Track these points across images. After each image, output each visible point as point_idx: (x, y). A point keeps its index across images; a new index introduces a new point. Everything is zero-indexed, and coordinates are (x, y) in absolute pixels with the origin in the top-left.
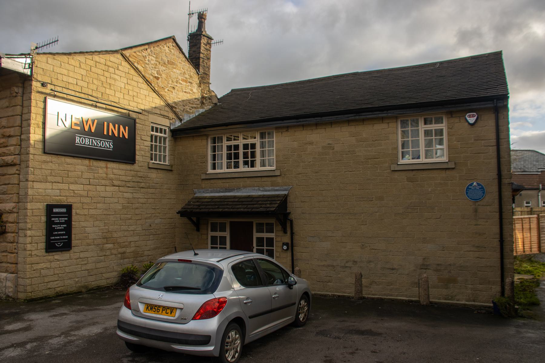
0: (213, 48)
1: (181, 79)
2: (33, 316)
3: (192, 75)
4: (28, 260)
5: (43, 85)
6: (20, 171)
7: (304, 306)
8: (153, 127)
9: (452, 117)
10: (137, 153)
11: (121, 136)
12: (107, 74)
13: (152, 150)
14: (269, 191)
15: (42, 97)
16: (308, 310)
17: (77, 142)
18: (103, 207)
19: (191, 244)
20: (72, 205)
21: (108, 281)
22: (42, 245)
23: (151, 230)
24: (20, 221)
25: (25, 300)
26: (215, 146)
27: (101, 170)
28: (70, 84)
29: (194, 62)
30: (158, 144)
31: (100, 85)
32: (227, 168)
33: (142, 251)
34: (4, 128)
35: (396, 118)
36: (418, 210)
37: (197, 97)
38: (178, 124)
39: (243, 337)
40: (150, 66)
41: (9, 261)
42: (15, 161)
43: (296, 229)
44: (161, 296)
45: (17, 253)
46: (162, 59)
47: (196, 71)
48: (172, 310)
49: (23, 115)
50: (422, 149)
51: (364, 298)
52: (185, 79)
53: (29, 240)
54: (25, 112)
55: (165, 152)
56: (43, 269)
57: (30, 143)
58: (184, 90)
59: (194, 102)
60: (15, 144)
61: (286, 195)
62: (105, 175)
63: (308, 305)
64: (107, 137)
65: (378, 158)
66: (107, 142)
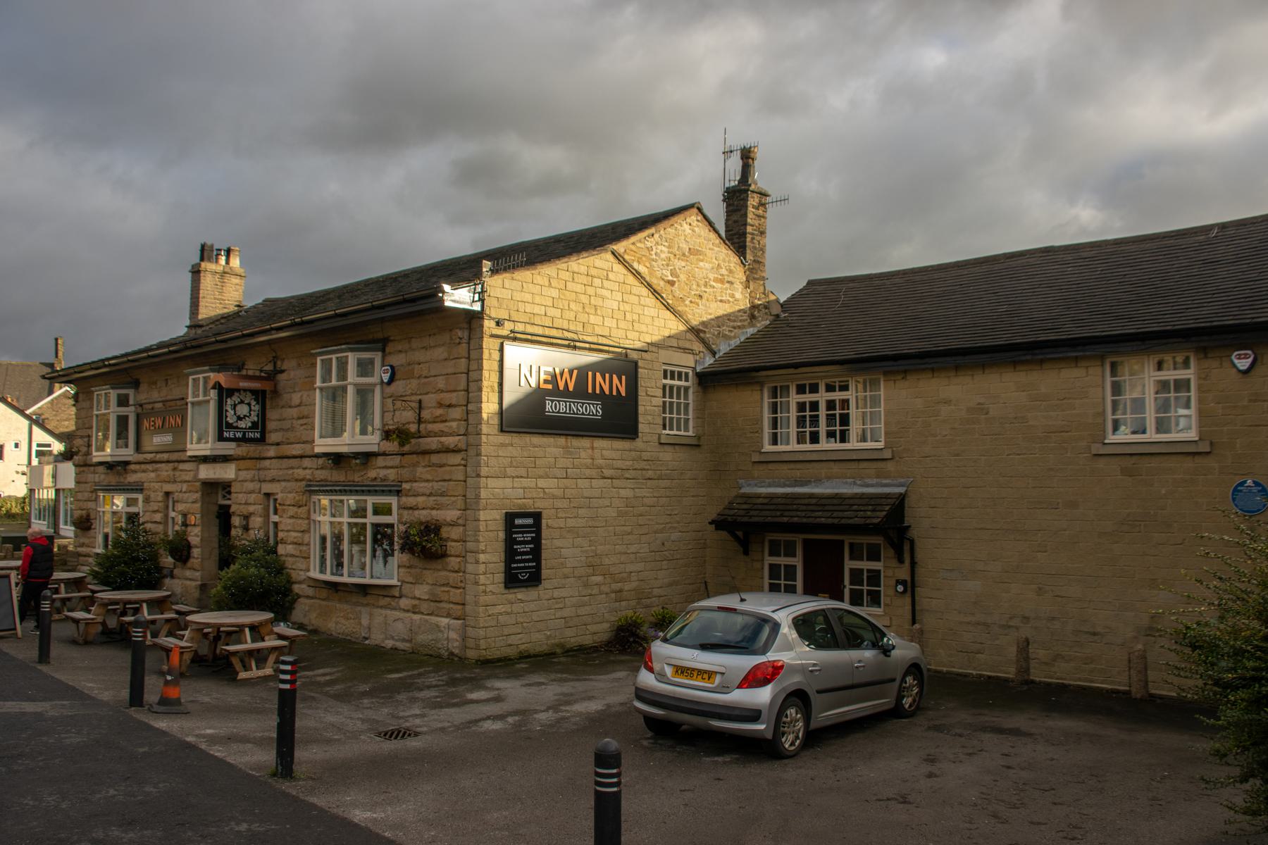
0: (772, 211)
2: (498, 684)
3: (732, 268)
4: (483, 599)
5: (499, 323)
7: (912, 686)
8: (665, 371)
9: (1206, 357)
10: (641, 419)
11: (615, 393)
12: (590, 291)
13: (664, 412)
14: (872, 486)
16: (920, 693)
19: (733, 578)
20: (541, 512)
21: (596, 638)
22: (500, 577)
24: (468, 539)
25: (477, 661)
29: (736, 240)
30: (675, 400)
31: (581, 310)
32: (798, 443)
35: (1102, 358)
36: (1142, 527)
37: (742, 307)
38: (709, 360)
39: (807, 718)
40: (660, 262)
41: (452, 599)
42: (460, 444)
43: (919, 555)
45: (464, 588)
48: (710, 674)
49: (470, 373)
50: (1150, 416)
51: (1033, 682)
52: (720, 277)
53: (482, 568)
55: (686, 413)
56: (501, 614)
57: (481, 418)
58: (719, 298)
59: (737, 317)
61: (901, 494)
62: (591, 461)
63: (921, 685)
64: (594, 396)
65: (1067, 432)
66: (593, 404)
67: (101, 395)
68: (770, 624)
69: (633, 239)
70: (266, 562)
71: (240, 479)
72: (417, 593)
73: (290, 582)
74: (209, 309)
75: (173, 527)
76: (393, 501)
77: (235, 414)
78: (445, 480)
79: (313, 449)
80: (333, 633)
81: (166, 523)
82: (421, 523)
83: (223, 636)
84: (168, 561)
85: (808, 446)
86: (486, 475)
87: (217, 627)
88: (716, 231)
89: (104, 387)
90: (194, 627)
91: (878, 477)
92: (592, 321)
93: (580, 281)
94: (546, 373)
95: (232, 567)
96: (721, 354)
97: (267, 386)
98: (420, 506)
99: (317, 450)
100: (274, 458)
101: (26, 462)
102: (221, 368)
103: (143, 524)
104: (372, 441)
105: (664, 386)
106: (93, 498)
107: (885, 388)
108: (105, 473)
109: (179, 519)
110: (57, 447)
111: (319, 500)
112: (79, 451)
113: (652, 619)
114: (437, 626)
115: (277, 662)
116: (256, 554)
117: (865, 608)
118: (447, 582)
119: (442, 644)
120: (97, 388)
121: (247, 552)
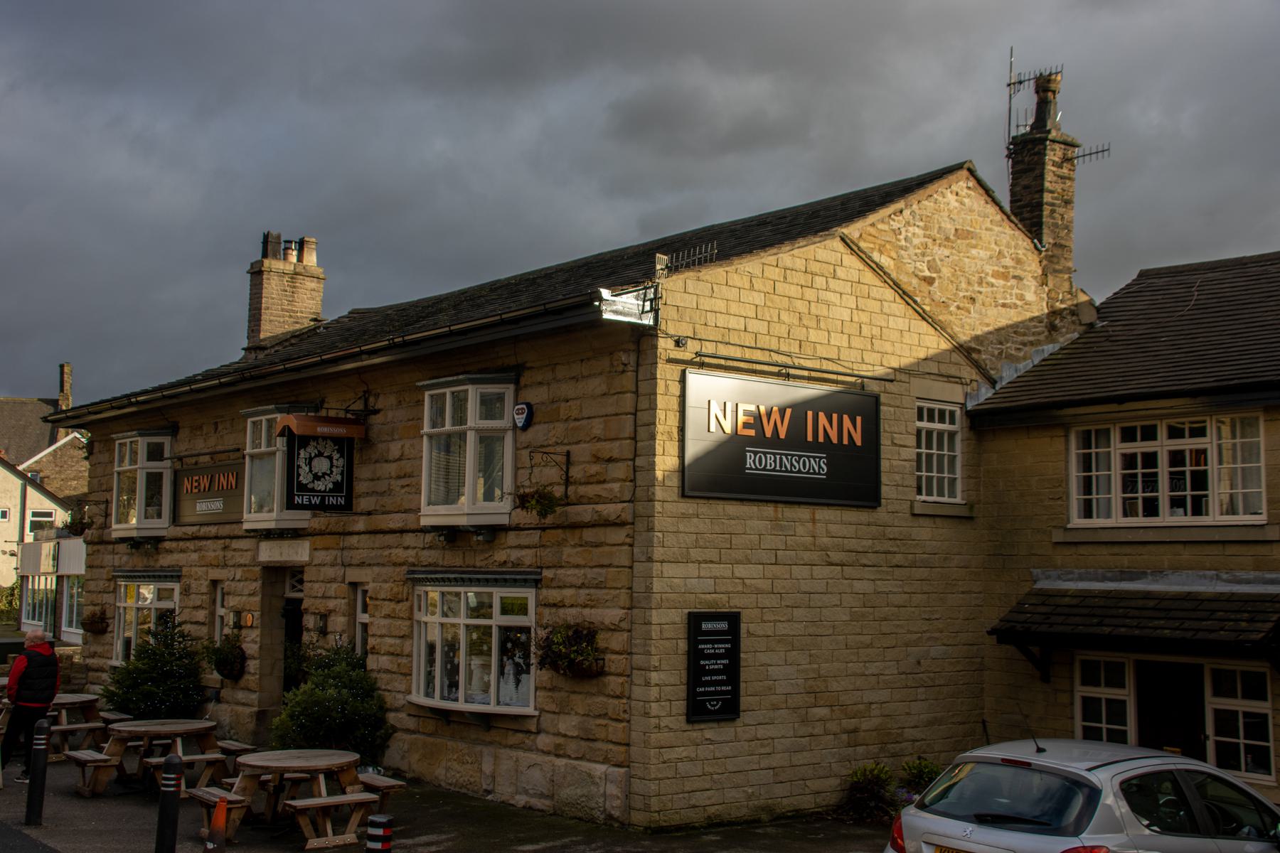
0: (1083, 170)
1: (990, 272)
3: (1021, 256)
5: (678, 343)
6: (633, 537)
8: (920, 410)
11: (845, 442)
12: (811, 295)
13: (919, 469)
14: (1248, 582)
15: (674, 371)
17: (748, 466)
18: (806, 616)
20: (739, 613)
22: (680, 706)
23: (921, 675)
25: (646, 828)
26: (1090, 454)
27: (800, 527)
28: (731, 331)
29: (1026, 215)
31: (796, 322)
32: (1125, 515)
33: (899, 728)
34: (597, 441)
37: (1036, 314)
38: (986, 393)
41: (611, 737)
42: (623, 515)
44: (968, 832)
45: (629, 722)
46: (940, 227)
47: (1033, 242)
49: (639, 413)
52: (1001, 270)
53: (654, 692)
54: (643, 408)
55: (952, 469)
56: (681, 760)
57: (654, 478)
58: (1001, 301)
60: (624, 478)
62: (811, 538)
64: (815, 447)
66: (814, 458)
67: (125, 444)
68: (1086, 790)
69: (872, 218)
70: (351, 680)
71: (316, 562)
72: (562, 728)
73: (383, 708)
74: (272, 327)
75: (222, 630)
76: (529, 594)
77: (311, 471)
78: (602, 566)
79: (418, 520)
80: (443, 784)
81: (212, 623)
82: (569, 627)
83: (288, 785)
84: (213, 677)
85: (1140, 521)
86: (661, 558)
87: (281, 771)
88: (996, 202)
89: (129, 434)
90: (248, 772)
91: (1257, 568)
92: (812, 338)
93: (795, 281)
94: (746, 413)
95: (303, 687)
96: (1004, 384)
97: (354, 432)
98: (567, 602)
99: (425, 522)
100: (364, 533)
101: (16, 538)
102: (292, 407)
103: (180, 624)
104: (500, 510)
105: (919, 431)
106: (111, 589)
107: (1267, 431)
108: (129, 554)
109: (231, 619)
110: (61, 517)
111: (427, 593)
112: (93, 522)
113: (903, 774)
114: (589, 775)
115: (364, 823)
116: (337, 669)
117: (1243, 774)
118: (605, 711)
119: (597, 803)
120: (120, 435)
121: (324, 664)
